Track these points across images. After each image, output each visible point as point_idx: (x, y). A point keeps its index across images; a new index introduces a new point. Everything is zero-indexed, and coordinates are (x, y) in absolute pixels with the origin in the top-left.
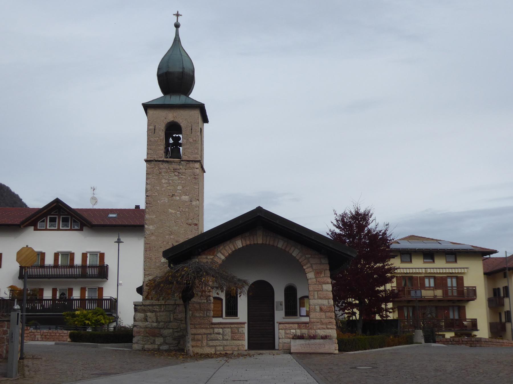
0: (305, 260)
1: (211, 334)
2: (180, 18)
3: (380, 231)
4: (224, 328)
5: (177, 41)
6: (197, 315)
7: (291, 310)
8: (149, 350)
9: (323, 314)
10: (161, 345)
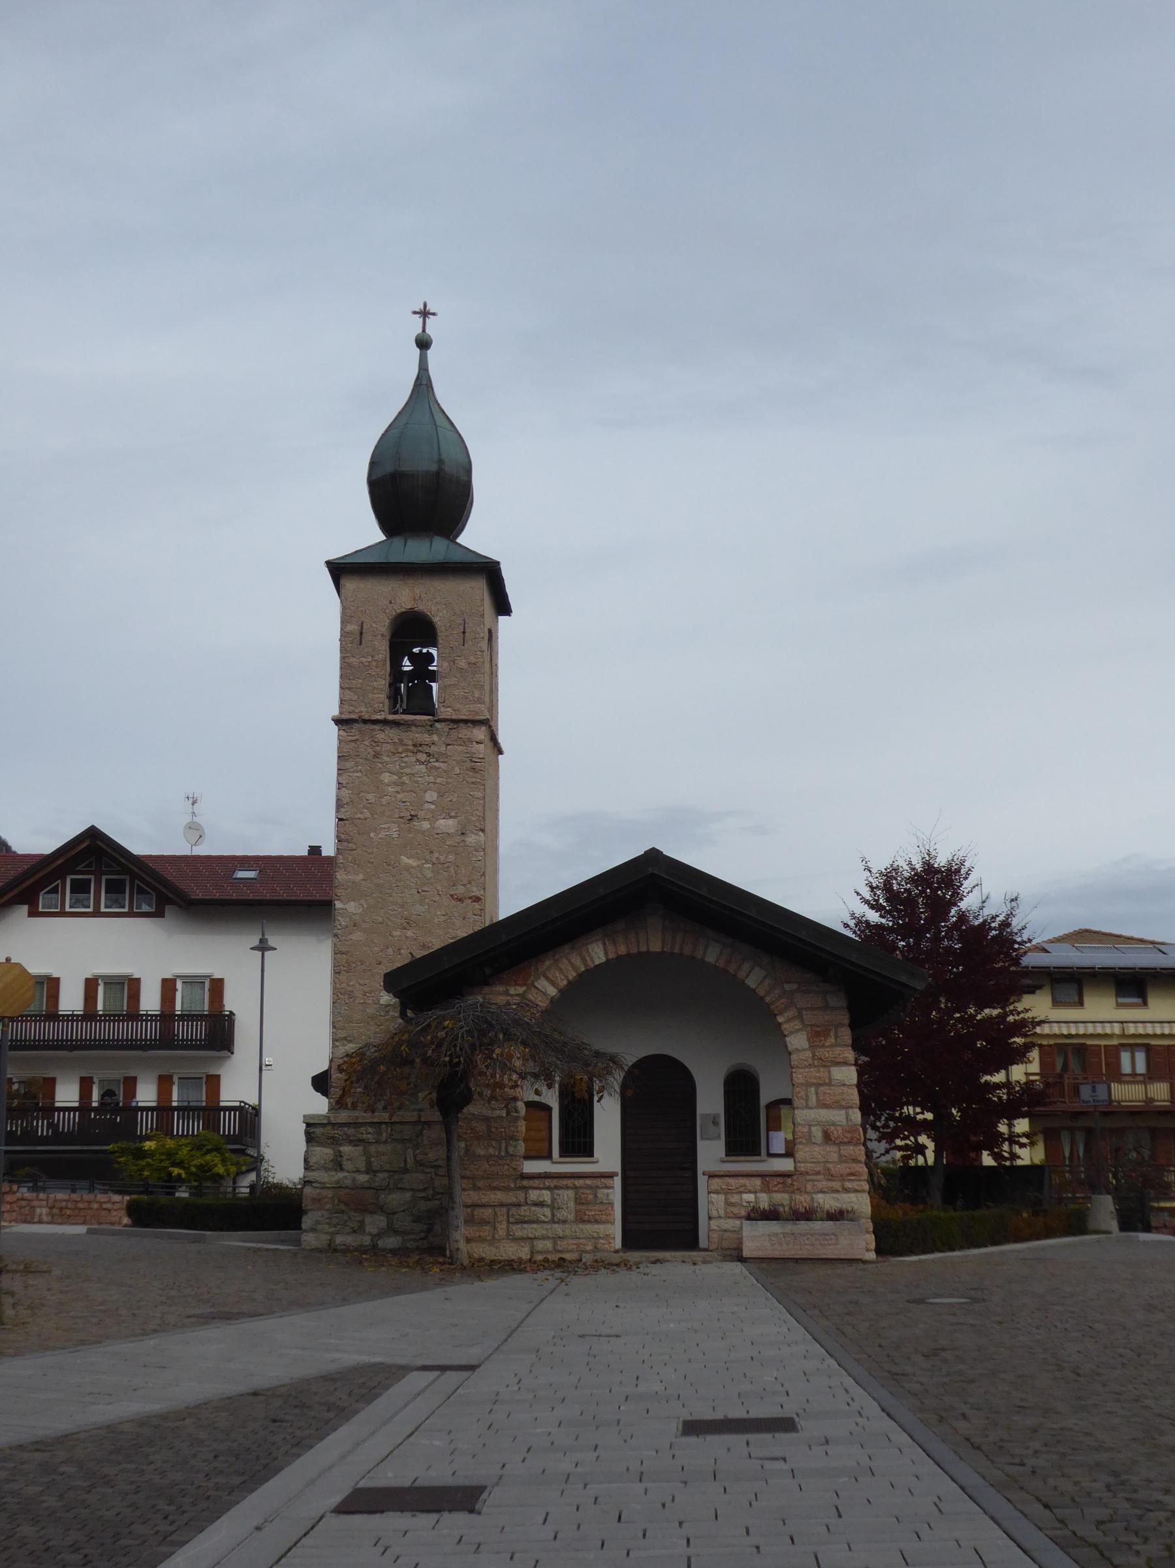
1: (519, 1205)
2: (430, 321)
3: (994, 918)
4: (556, 1187)
5: (423, 385)
7: (744, 1138)
8: (346, 1250)
9: (834, 1149)
10: (379, 1235)
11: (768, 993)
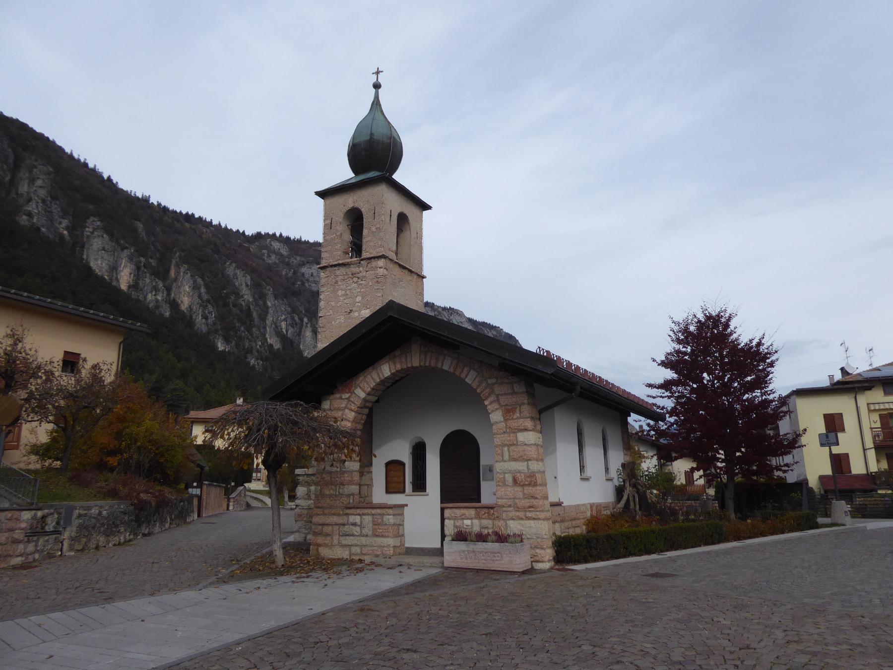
0: (486, 388)
1: (344, 525)
2: (380, 75)
3: (751, 341)
4: (363, 514)
5: (376, 104)
6: (327, 492)
9: (520, 489)
11: (478, 386)
